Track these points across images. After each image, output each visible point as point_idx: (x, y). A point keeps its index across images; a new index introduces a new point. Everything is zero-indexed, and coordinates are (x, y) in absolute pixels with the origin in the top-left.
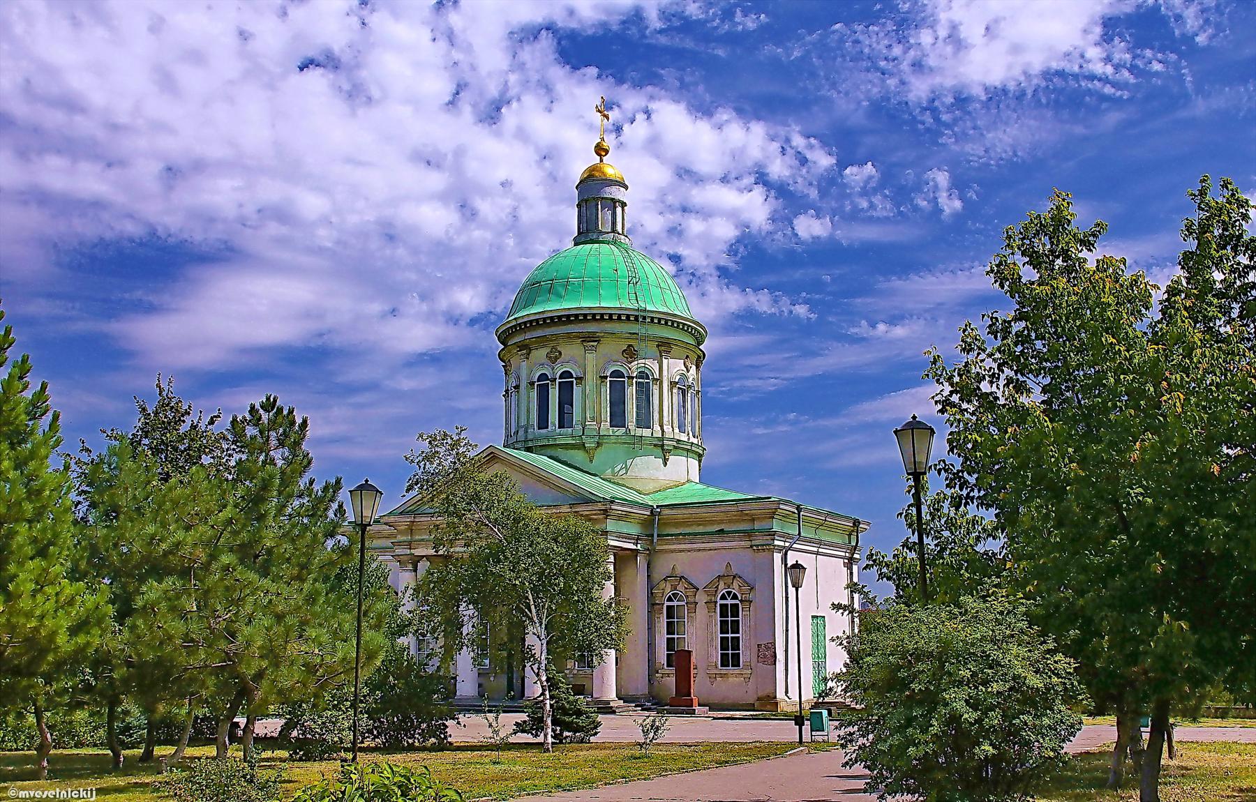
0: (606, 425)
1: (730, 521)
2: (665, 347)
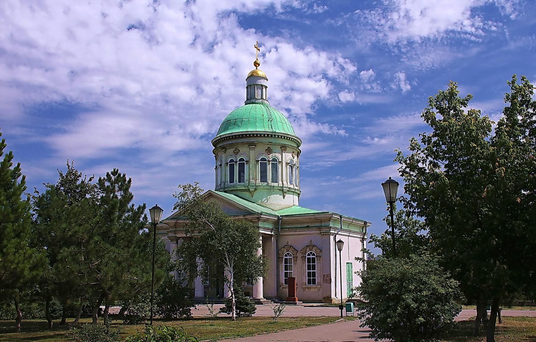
0: (259, 181)
1: (312, 222)
2: (284, 148)
